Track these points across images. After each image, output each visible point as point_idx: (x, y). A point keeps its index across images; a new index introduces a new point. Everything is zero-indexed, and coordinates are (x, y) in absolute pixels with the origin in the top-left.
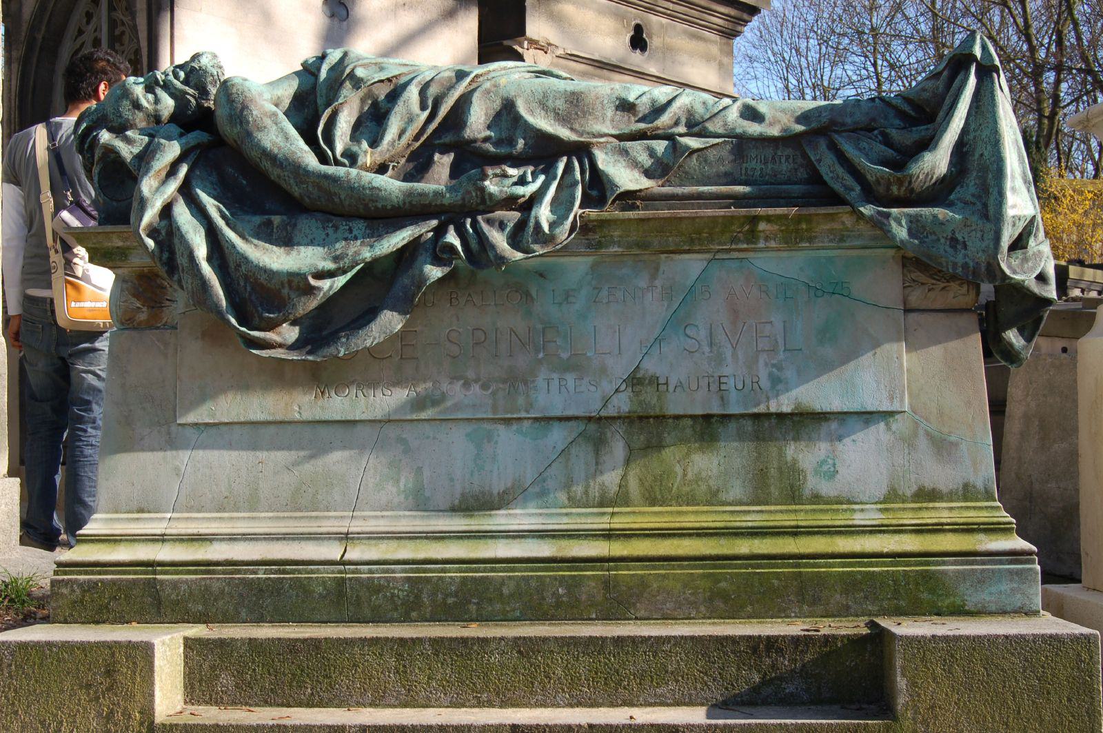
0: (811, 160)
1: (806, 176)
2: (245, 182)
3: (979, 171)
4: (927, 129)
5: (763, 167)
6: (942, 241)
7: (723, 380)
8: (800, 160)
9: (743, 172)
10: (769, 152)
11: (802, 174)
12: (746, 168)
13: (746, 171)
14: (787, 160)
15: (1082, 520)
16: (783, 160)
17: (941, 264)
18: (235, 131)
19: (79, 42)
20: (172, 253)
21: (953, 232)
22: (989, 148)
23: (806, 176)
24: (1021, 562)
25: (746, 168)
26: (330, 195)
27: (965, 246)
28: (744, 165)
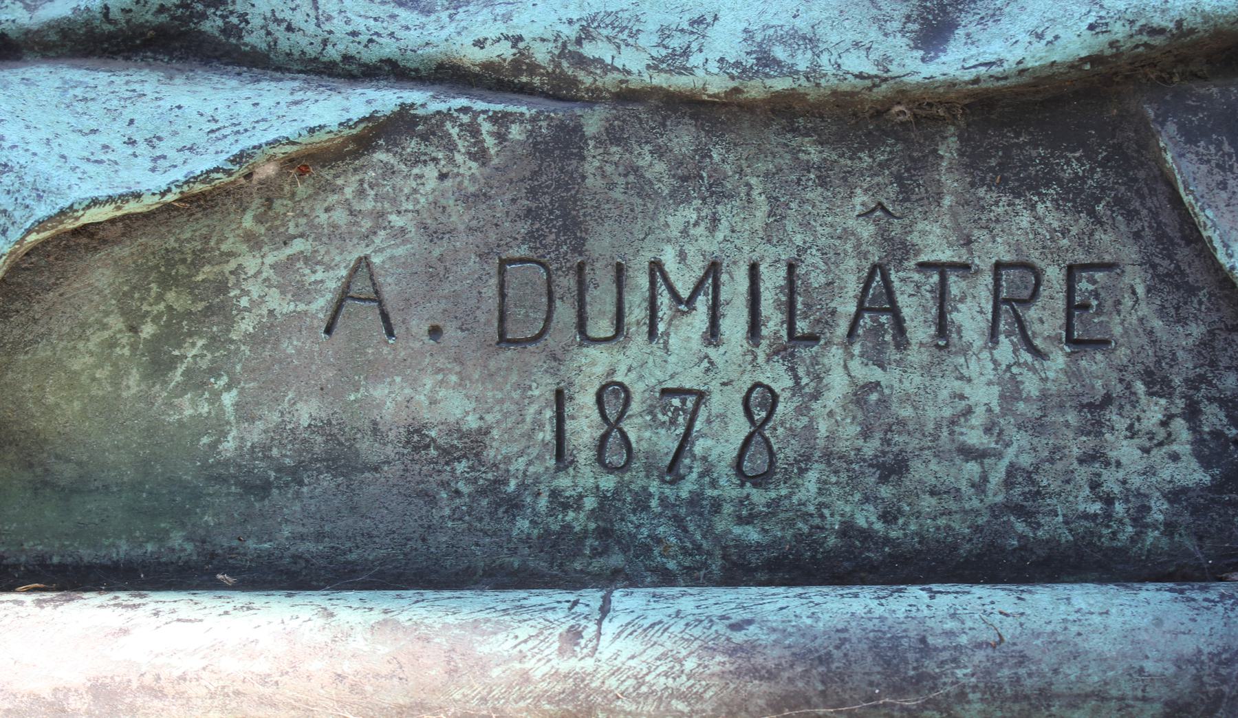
1: (1192, 474)
2: (163, 525)
5: (777, 377)
8: (1135, 312)
9: (584, 426)
10: (836, 231)
12: (612, 394)
13: (612, 426)
14: (1010, 309)
15: (258, 599)
16: (970, 318)
23: (1192, 474)
25: (612, 394)
28: (595, 364)
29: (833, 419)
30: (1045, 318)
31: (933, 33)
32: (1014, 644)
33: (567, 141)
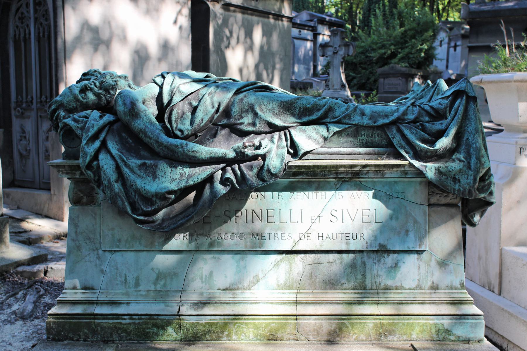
0: (389, 138)
3: (466, 146)
4: (441, 124)
6: (449, 179)
7: (348, 235)
8: (384, 136)
10: (370, 132)
11: (384, 142)
12: (360, 139)
17: (448, 189)
18: (127, 118)
19: (19, 4)
20: (100, 176)
21: (455, 175)
22: (472, 136)
24: (476, 319)
25: (360, 139)
26: (173, 151)
27: (459, 181)
29: (370, 140)
30: (380, 136)
31: (375, 123)
32: (455, 179)
33: (358, 128)
